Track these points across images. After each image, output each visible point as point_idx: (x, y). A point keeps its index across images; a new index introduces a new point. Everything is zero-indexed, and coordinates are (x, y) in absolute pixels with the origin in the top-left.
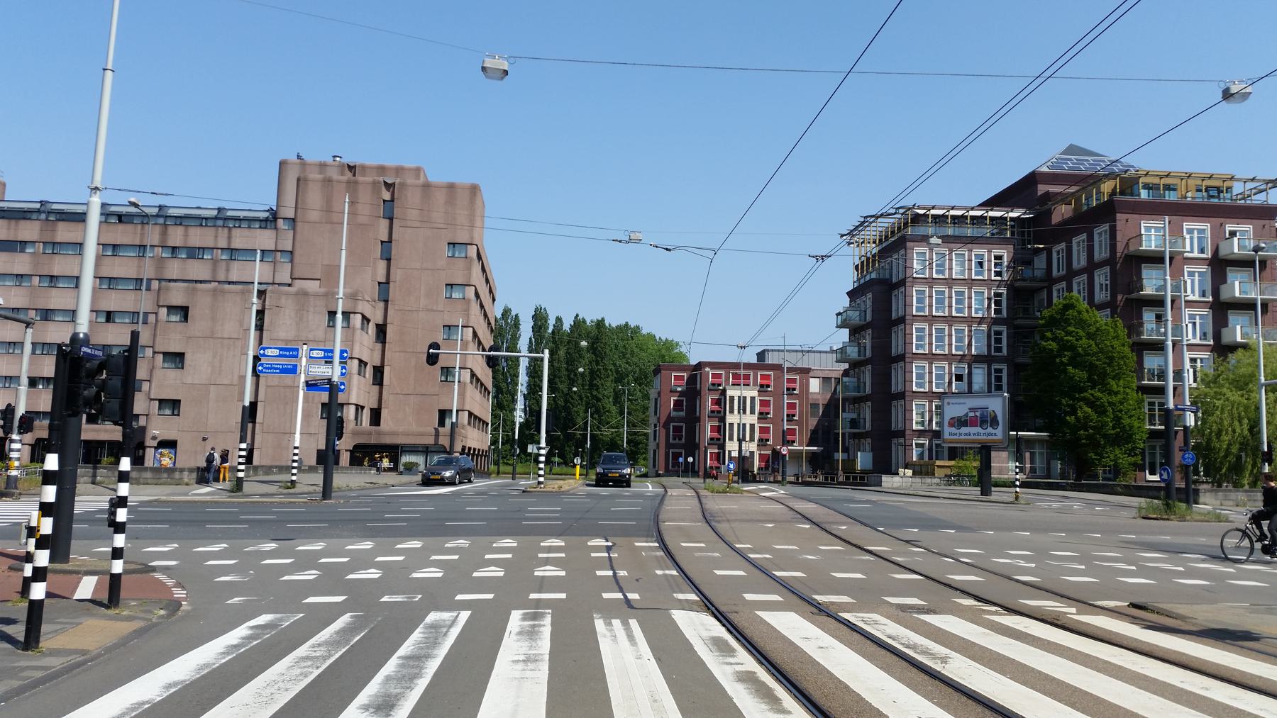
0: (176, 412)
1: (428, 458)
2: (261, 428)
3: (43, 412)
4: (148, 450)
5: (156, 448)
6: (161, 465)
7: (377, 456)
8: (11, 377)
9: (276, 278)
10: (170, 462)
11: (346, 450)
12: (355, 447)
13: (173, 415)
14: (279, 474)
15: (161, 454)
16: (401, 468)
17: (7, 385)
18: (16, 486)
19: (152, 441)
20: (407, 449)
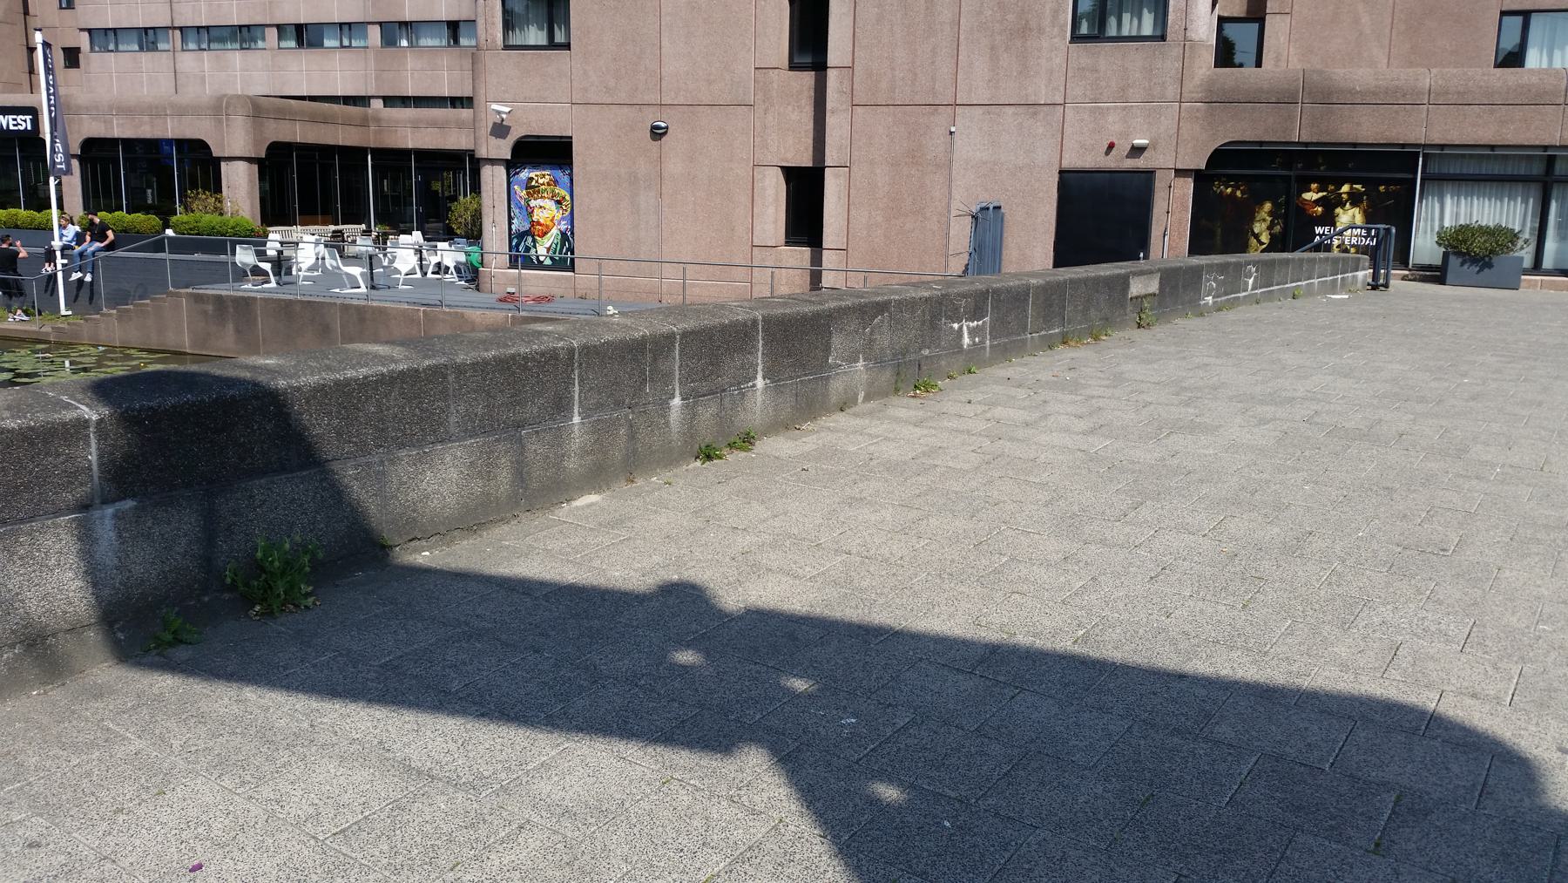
0: (559, 37)
1: (1554, 207)
2: (846, 87)
3: (414, 97)
4: (487, 172)
5: (512, 166)
6: (533, 223)
7: (1310, 196)
8: (349, 24)
9: (833, 70)
10: (559, 216)
11: (1180, 173)
12: (1221, 157)
13: (552, 45)
14: (1004, 353)
15: (529, 186)
16: (1424, 246)
17: (346, 43)
18: (1296, 80)
19: (493, 141)
20: (1454, 169)
